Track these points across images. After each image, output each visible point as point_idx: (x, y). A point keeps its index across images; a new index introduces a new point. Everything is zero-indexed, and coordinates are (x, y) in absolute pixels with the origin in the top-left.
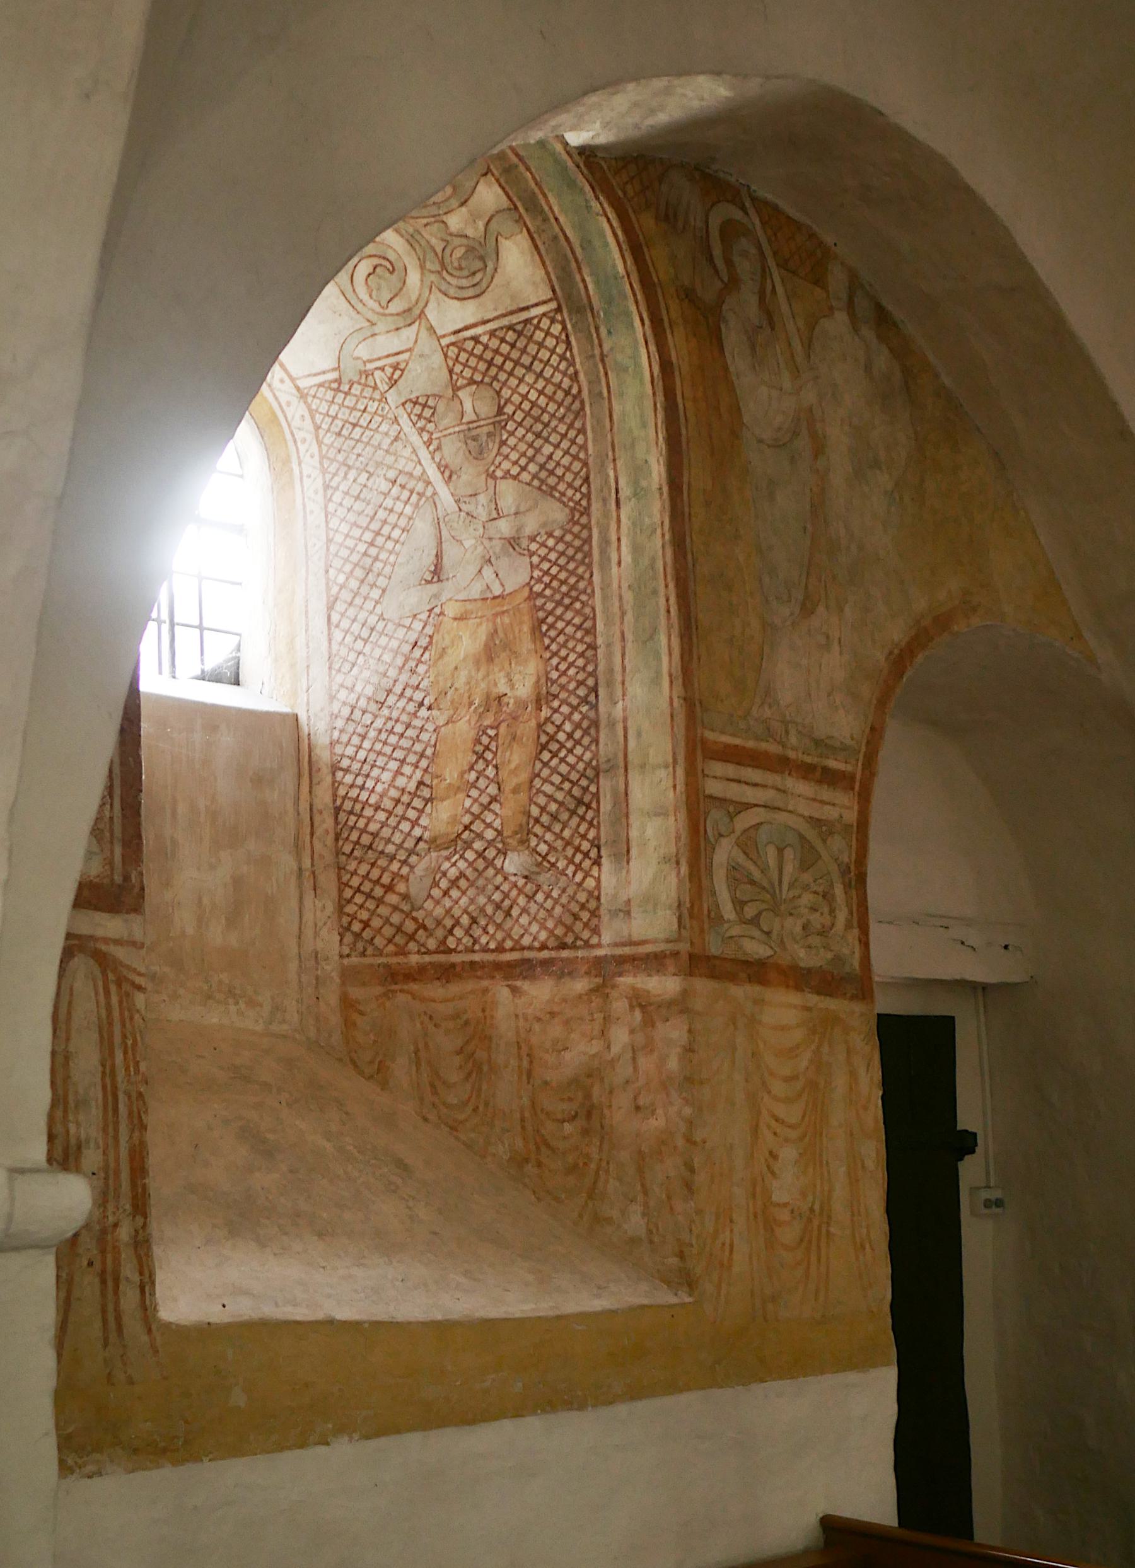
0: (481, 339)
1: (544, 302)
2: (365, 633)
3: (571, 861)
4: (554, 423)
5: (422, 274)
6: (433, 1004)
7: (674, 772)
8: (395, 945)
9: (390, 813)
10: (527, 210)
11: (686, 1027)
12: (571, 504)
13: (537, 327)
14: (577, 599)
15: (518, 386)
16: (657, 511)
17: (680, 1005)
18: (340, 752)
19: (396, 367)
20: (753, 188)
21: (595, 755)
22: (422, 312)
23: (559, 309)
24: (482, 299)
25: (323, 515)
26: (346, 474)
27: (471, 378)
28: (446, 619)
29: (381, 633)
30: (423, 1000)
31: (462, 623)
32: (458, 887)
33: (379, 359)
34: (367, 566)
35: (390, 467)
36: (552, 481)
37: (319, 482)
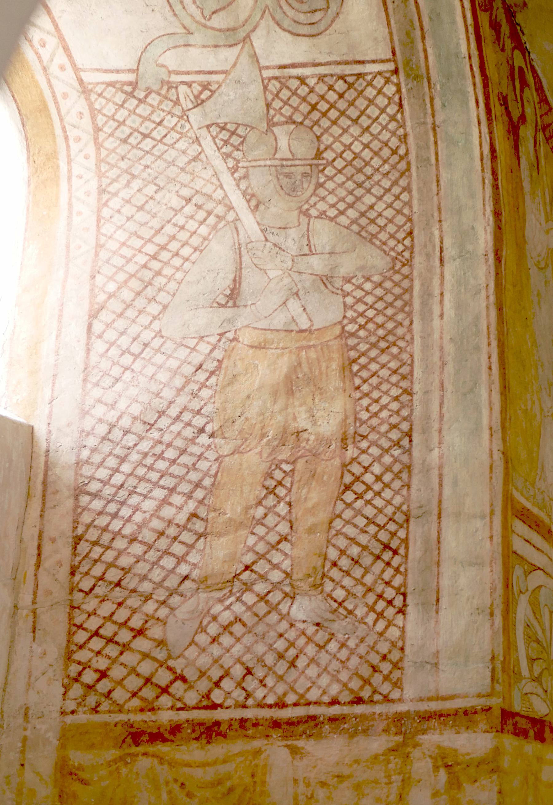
0: (308, 81)
1: (382, 61)
2: (136, 348)
3: (372, 609)
4: (377, 177)
6: (186, 770)
7: (491, 522)
8: (142, 699)
9: (150, 547)
11: (496, 789)
12: (393, 254)
13: (370, 84)
14: (394, 344)
15: (341, 135)
16: (483, 273)
17: (490, 764)
18: (89, 474)
19: (205, 86)
21: (407, 500)
22: (247, 38)
23: (396, 71)
24: (315, 40)
25: (94, 219)
26: (129, 182)
27: (290, 117)
28: (240, 345)
29: (157, 351)
30: (172, 764)
31: (259, 352)
32: (231, 633)
33: (188, 73)
34: (147, 279)
35: (183, 185)
36: (373, 229)
37: (94, 185)
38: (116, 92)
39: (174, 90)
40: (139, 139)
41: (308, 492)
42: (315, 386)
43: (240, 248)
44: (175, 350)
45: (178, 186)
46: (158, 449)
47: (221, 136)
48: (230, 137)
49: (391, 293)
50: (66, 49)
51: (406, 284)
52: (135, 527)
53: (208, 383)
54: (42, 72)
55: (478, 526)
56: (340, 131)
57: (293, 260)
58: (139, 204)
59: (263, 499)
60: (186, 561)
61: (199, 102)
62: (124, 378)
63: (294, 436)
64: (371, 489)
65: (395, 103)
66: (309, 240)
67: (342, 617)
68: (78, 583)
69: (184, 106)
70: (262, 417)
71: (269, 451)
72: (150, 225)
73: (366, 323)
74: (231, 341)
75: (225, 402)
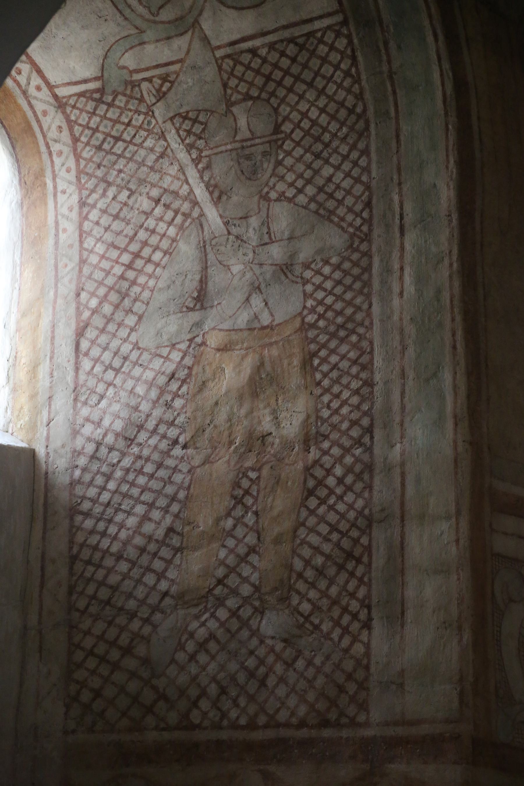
1: (329, 15)
3: (337, 623)
4: (335, 144)
12: (351, 230)
13: (321, 41)
14: (353, 332)
15: (297, 103)
16: (444, 238)
18: (81, 494)
19: (164, 79)
22: (196, 22)
23: (345, 23)
25: (77, 234)
26: (105, 191)
27: (247, 93)
28: (209, 349)
29: (135, 363)
33: (147, 69)
35: (153, 185)
36: (331, 204)
37: (75, 198)
38: (87, 102)
39: (137, 89)
41: (273, 500)
42: (278, 386)
43: (205, 246)
44: (151, 361)
45: (149, 186)
47: (184, 127)
48: (192, 126)
50: (39, 72)
53: (180, 393)
54: (22, 96)
56: (296, 99)
57: (254, 252)
59: (231, 510)
61: (161, 95)
62: (108, 394)
63: (260, 441)
66: (269, 228)
67: (309, 632)
69: (148, 102)
70: (229, 423)
71: (236, 459)
72: (125, 232)
73: (325, 311)
74: (200, 345)
75: (196, 410)
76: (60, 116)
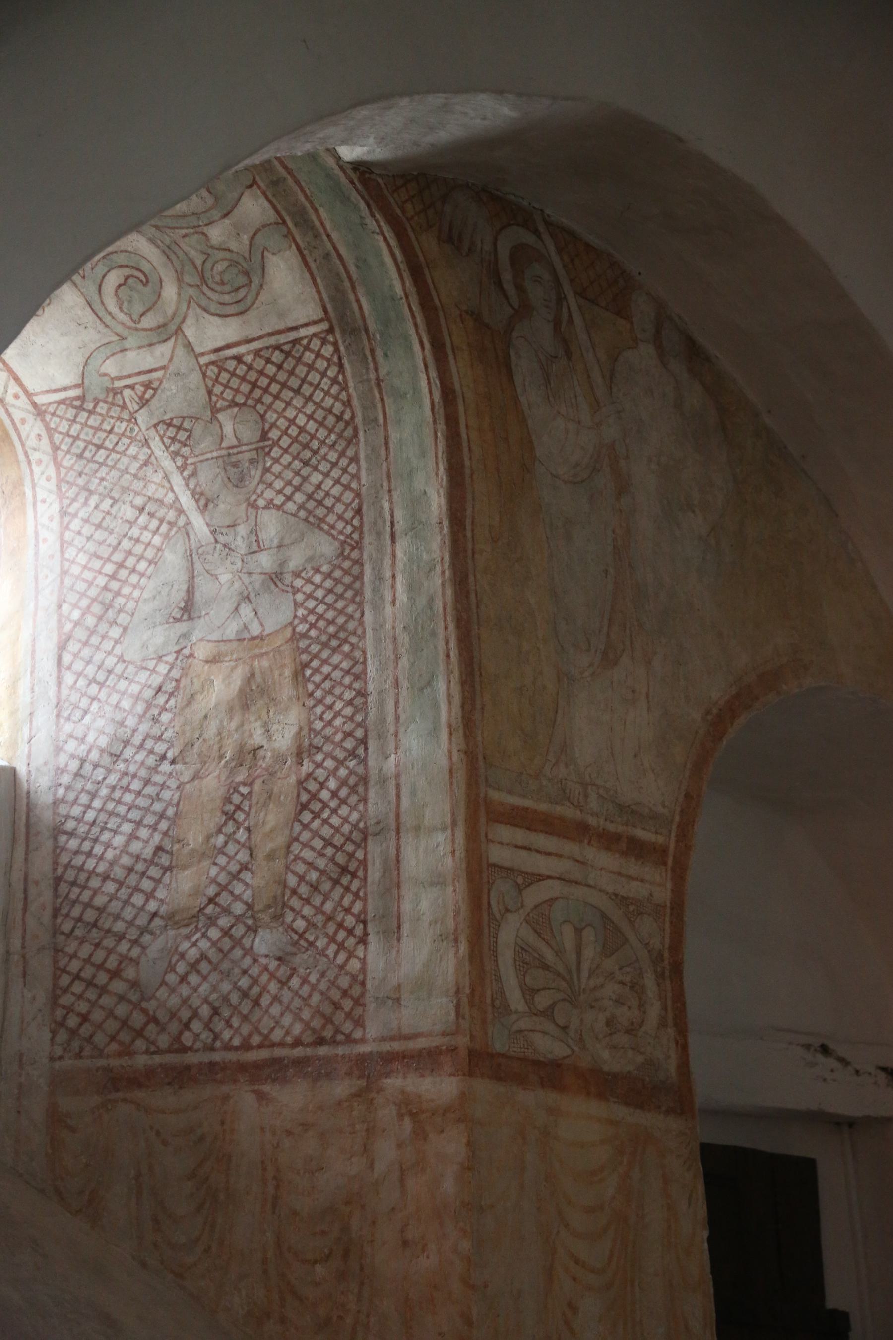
1: (315, 322)
3: (332, 939)
4: (323, 451)
5: (180, 288)
10: (296, 225)
12: (342, 538)
13: (307, 348)
14: (346, 641)
15: (284, 410)
16: (436, 546)
19: (147, 386)
20: (548, 212)
22: (179, 328)
23: (331, 330)
26: (87, 499)
27: (233, 401)
28: (196, 661)
31: (214, 667)
33: (129, 376)
34: (107, 601)
35: (137, 493)
36: (321, 512)
37: (56, 507)
39: (119, 396)
40: (93, 452)
41: (266, 815)
43: (191, 555)
44: (136, 673)
45: (132, 494)
46: (124, 782)
49: (342, 583)
51: (356, 570)
52: (107, 865)
55: (439, 839)
56: (283, 406)
57: (243, 561)
58: (97, 522)
59: (222, 826)
60: (154, 897)
62: (92, 709)
64: (328, 807)
65: (335, 364)
66: (257, 535)
67: (303, 950)
68: (60, 925)
72: (108, 542)
73: (317, 620)
74: (187, 657)
76: (39, 424)
